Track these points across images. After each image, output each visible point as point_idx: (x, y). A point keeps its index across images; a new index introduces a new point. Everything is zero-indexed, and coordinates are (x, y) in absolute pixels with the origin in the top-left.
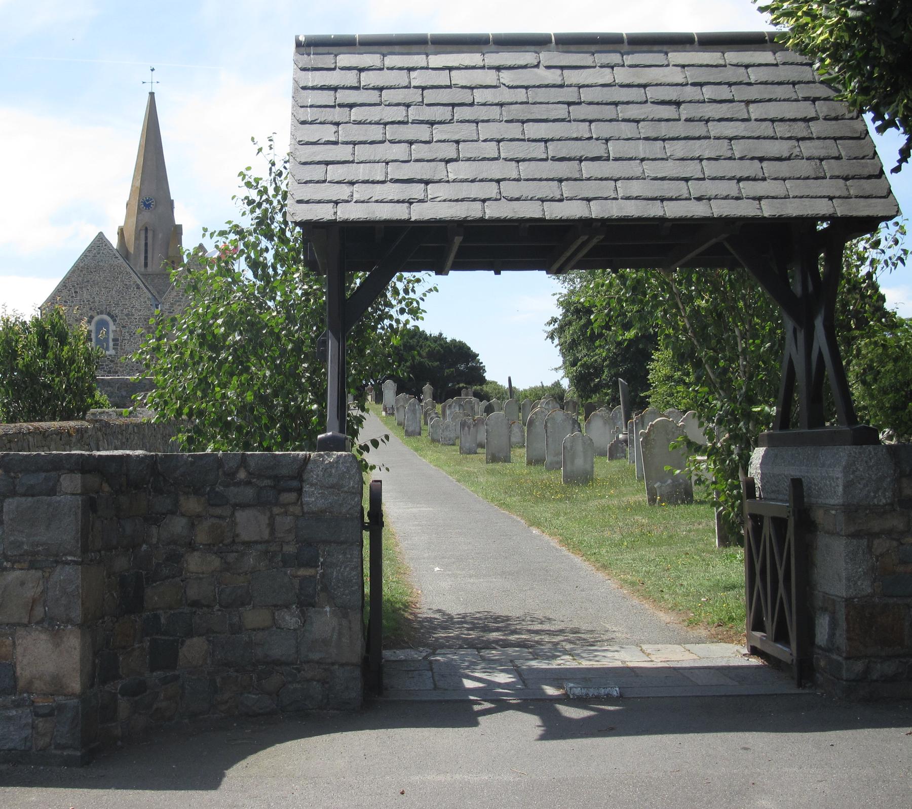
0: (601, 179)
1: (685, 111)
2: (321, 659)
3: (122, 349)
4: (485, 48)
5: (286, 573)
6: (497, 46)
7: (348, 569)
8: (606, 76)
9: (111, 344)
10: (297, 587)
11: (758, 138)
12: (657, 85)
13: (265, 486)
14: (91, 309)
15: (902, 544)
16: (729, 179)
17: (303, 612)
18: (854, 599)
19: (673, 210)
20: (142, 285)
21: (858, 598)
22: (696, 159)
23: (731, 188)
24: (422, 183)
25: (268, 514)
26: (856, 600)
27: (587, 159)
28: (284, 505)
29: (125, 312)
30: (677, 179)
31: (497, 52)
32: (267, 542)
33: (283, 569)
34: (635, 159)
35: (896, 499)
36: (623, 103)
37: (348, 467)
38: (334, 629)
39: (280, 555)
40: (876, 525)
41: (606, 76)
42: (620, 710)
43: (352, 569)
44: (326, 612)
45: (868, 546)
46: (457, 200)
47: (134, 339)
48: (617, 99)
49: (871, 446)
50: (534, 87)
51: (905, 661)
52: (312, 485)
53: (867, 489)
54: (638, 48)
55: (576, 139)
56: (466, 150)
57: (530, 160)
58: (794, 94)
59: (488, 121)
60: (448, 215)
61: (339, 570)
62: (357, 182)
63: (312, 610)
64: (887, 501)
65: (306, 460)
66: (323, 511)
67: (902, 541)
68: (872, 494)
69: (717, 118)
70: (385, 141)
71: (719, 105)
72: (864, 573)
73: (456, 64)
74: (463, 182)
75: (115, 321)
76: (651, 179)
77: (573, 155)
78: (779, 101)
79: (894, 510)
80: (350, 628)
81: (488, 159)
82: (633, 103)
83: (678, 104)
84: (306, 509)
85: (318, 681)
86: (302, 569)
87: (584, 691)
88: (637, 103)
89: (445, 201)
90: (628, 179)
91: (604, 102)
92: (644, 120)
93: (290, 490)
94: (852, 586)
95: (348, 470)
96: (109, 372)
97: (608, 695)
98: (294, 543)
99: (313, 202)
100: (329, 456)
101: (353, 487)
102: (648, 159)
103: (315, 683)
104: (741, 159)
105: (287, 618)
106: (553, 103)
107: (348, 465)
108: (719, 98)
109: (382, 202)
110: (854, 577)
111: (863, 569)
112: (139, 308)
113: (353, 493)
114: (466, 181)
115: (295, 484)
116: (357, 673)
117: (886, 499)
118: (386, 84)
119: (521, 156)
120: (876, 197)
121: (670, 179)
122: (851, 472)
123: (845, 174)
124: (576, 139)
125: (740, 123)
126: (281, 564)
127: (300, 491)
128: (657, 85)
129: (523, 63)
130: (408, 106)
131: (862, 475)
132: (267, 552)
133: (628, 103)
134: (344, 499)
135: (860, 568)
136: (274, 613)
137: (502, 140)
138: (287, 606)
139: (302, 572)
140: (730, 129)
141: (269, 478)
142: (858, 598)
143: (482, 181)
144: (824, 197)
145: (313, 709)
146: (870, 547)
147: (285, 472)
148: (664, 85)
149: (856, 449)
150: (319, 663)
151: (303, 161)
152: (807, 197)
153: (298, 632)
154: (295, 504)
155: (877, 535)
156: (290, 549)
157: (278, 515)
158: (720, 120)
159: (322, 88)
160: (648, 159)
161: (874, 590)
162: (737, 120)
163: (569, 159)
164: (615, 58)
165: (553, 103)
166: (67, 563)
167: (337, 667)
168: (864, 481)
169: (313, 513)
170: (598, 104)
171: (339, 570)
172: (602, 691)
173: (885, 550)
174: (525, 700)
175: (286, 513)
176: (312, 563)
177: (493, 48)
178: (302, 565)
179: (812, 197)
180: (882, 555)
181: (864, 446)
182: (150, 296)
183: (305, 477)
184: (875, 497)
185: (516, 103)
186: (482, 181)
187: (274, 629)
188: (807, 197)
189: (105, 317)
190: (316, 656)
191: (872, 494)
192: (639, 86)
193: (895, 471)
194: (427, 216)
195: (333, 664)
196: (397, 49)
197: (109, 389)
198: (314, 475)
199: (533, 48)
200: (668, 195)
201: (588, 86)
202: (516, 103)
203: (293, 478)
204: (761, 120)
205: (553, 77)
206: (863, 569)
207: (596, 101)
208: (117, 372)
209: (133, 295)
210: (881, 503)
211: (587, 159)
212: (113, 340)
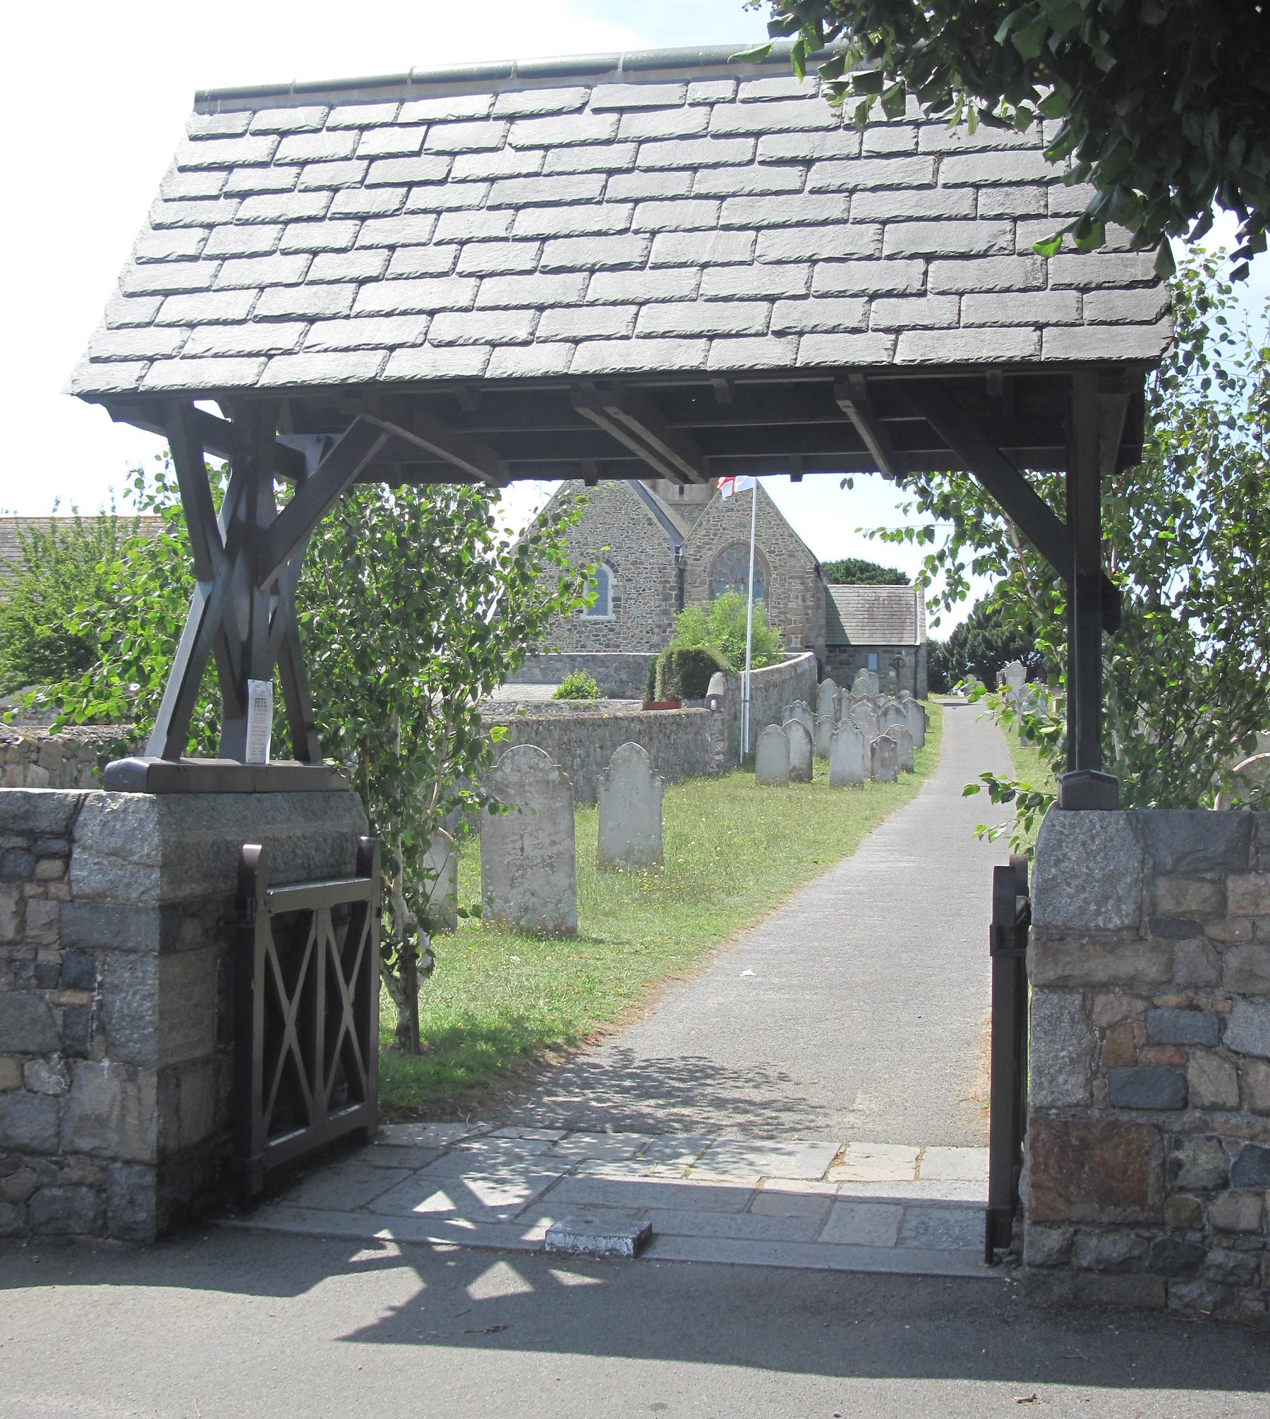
0: (614, 303)
1: (817, 176)
2: (94, 1149)
3: (625, 612)
4: (501, 85)
5: (42, 998)
6: (522, 80)
7: (138, 997)
8: (692, 120)
9: (611, 604)
10: (60, 1022)
11: (937, 219)
12: (780, 131)
13: (14, 848)
14: (582, 554)
15: (1156, 1007)
16: (854, 296)
17: (68, 1067)
18: (1049, 1108)
19: (724, 356)
20: (655, 520)
21: (1058, 1108)
22: (805, 261)
23: (851, 312)
24: (302, 321)
25: (16, 896)
26: (1054, 1111)
27: (603, 268)
28: (45, 882)
29: (632, 558)
30: (755, 299)
31: (520, 91)
32: (11, 943)
33: (38, 991)
34: (691, 265)
35: (1146, 919)
36: (708, 166)
37: (141, 819)
38: (114, 1099)
39: (32, 967)
40: (1101, 967)
41: (692, 120)
42: (585, 1287)
43: (144, 998)
44: (102, 1068)
45: (1083, 1008)
46: (347, 349)
47: (644, 598)
48: (697, 160)
49: (1097, 812)
50: (560, 146)
51: (1147, 1234)
52: (85, 849)
53: (1083, 896)
54: (770, 68)
55: (599, 233)
56: (404, 262)
57: (502, 274)
58: (1037, 135)
59: (458, 209)
60: (318, 376)
61: (125, 998)
62: (200, 323)
63: (82, 1063)
64: (1122, 922)
65: (79, 804)
66: (101, 895)
67: (1157, 1001)
68: (1093, 907)
69: (871, 184)
70: (274, 252)
71: (885, 162)
72: (1072, 1061)
73: (440, 115)
74: (373, 316)
75: (616, 571)
76: (706, 301)
77: (579, 263)
78: (1002, 150)
79: (1142, 939)
80: (139, 1100)
81: (432, 275)
82: (725, 165)
83: (808, 163)
84: (75, 890)
85: (91, 1186)
86: (68, 993)
87: (570, 1241)
88: (733, 165)
89: (326, 351)
90: (664, 301)
91: (674, 166)
92: (734, 195)
93: (53, 856)
94: (1046, 1084)
95: (140, 824)
96: (608, 646)
97: (611, 1250)
98: (56, 946)
99: (116, 361)
100: (114, 799)
101: (148, 855)
102: (716, 265)
103: (84, 1189)
104: (891, 257)
105: (44, 1074)
106: (582, 173)
107: (142, 816)
108: (885, 150)
109: (223, 356)
110: (1051, 1066)
111: (1070, 1053)
112: (651, 552)
113: (148, 866)
114: (378, 314)
115: (59, 845)
116: (150, 1179)
117: (1120, 917)
118: (312, 156)
119: (487, 267)
120: (1131, 323)
121: (741, 299)
122: (1052, 863)
123: (1081, 280)
124: (599, 233)
125: (914, 192)
126: (34, 982)
127: (67, 857)
128: (780, 131)
129: (555, 106)
130: (335, 190)
131: (1073, 870)
132: (10, 961)
133: (716, 166)
134: (132, 875)
135: (1063, 1050)
136: (23, 1066)
137: (468, 241)
138: (45, 1056)
139: (69, 997)
140: (887, 205)
141: (21, 833)
142: (1058, 1108)
143: (404, 313)
144: (1026, 325)
145: (80, 1234)
146: (1087, 1013)
147: (43, 824)
148: (793, 131)
149: (1065, 817)
150: (92, 1155)
151: (131, 290)
152: (994, 325)
153: (61, 1099)
154: (60, 879)
155: (1105, 987)
156: (50, 957)
157: (32, 897)
158: (874, 189)
159: (210, 168)
160: (716, 265)
161: (1092, 1095)
162: (909, 187)
163: (572, 270)
164: (723, 88)
165: (582, 173)
166: (1204, 880)
167: (118, 1165)
168: (1075, 882)
169: (86, 897)
170: (662, 169)
171: (125, 998)
172: (603, 1244)
173: (1118, 1017)
174: (464, 1247)
175: (46, 896)
176: (82, 983)
177: (517, 83)
178: (75, 985)
179: (1002, 326)
180: (1112, 1026)
181: (1082, 812)
182: (667, 535)
183: (77, 835)
184: (1098, 913)
185: (519, 176)
186: (404, 313)
187: (23, 1091)
188: (994, 325)
189: (605, 567)
190: (85, 1144)
191: (1093, 907)
192: (747, 134)
193: (1143, 862)
194: (282, 380)
195: (114, 1159)
196: (355, 94)
197: (602, 669)
198: (88, 830)
199: (583, 79)
200: (723, 327)
201: (655, 139)
202: (519, 176)
203: (58, 836)
204: (956, 186)
205: (601, 126)
206: (1070, 1053)
207: (659, 164)
208: (618, 646)
209: (642, 535)
210: (1111, 926)
211: (603, 268)
212: (614, 599)
